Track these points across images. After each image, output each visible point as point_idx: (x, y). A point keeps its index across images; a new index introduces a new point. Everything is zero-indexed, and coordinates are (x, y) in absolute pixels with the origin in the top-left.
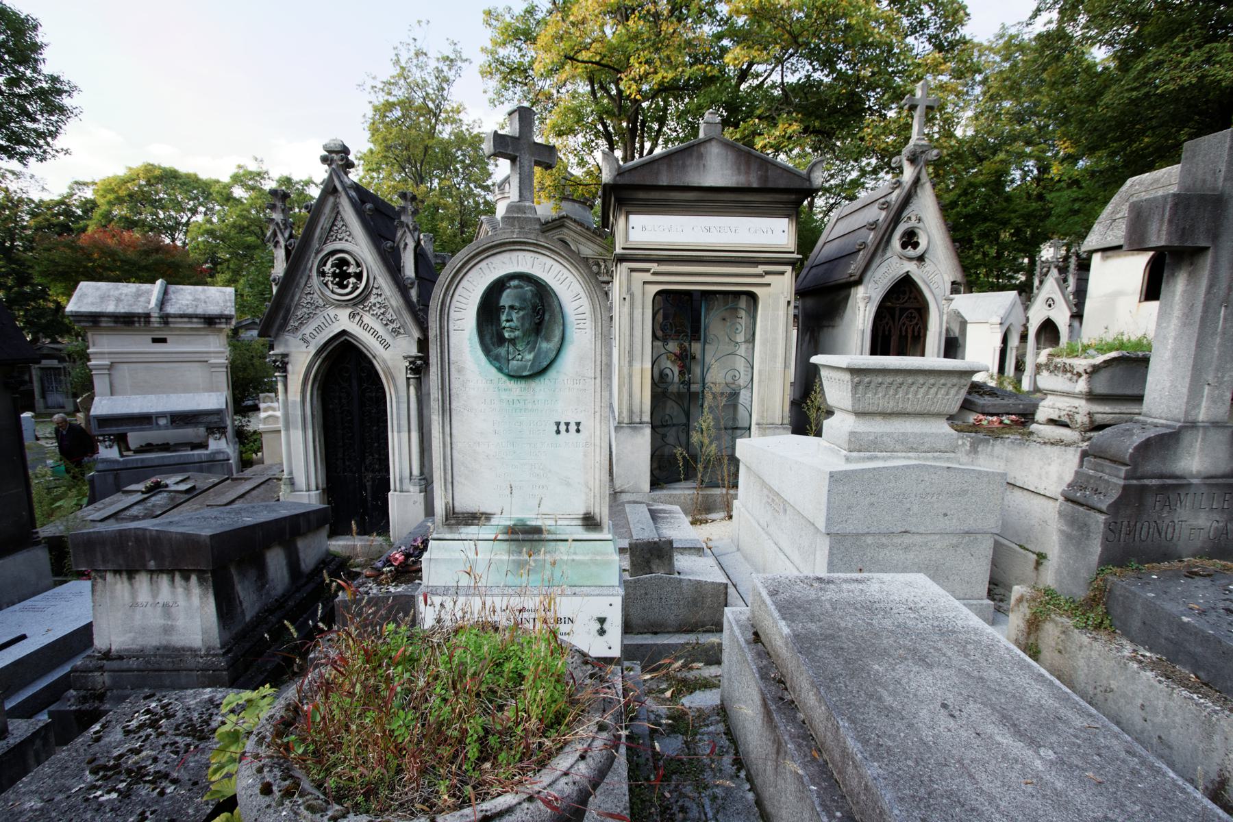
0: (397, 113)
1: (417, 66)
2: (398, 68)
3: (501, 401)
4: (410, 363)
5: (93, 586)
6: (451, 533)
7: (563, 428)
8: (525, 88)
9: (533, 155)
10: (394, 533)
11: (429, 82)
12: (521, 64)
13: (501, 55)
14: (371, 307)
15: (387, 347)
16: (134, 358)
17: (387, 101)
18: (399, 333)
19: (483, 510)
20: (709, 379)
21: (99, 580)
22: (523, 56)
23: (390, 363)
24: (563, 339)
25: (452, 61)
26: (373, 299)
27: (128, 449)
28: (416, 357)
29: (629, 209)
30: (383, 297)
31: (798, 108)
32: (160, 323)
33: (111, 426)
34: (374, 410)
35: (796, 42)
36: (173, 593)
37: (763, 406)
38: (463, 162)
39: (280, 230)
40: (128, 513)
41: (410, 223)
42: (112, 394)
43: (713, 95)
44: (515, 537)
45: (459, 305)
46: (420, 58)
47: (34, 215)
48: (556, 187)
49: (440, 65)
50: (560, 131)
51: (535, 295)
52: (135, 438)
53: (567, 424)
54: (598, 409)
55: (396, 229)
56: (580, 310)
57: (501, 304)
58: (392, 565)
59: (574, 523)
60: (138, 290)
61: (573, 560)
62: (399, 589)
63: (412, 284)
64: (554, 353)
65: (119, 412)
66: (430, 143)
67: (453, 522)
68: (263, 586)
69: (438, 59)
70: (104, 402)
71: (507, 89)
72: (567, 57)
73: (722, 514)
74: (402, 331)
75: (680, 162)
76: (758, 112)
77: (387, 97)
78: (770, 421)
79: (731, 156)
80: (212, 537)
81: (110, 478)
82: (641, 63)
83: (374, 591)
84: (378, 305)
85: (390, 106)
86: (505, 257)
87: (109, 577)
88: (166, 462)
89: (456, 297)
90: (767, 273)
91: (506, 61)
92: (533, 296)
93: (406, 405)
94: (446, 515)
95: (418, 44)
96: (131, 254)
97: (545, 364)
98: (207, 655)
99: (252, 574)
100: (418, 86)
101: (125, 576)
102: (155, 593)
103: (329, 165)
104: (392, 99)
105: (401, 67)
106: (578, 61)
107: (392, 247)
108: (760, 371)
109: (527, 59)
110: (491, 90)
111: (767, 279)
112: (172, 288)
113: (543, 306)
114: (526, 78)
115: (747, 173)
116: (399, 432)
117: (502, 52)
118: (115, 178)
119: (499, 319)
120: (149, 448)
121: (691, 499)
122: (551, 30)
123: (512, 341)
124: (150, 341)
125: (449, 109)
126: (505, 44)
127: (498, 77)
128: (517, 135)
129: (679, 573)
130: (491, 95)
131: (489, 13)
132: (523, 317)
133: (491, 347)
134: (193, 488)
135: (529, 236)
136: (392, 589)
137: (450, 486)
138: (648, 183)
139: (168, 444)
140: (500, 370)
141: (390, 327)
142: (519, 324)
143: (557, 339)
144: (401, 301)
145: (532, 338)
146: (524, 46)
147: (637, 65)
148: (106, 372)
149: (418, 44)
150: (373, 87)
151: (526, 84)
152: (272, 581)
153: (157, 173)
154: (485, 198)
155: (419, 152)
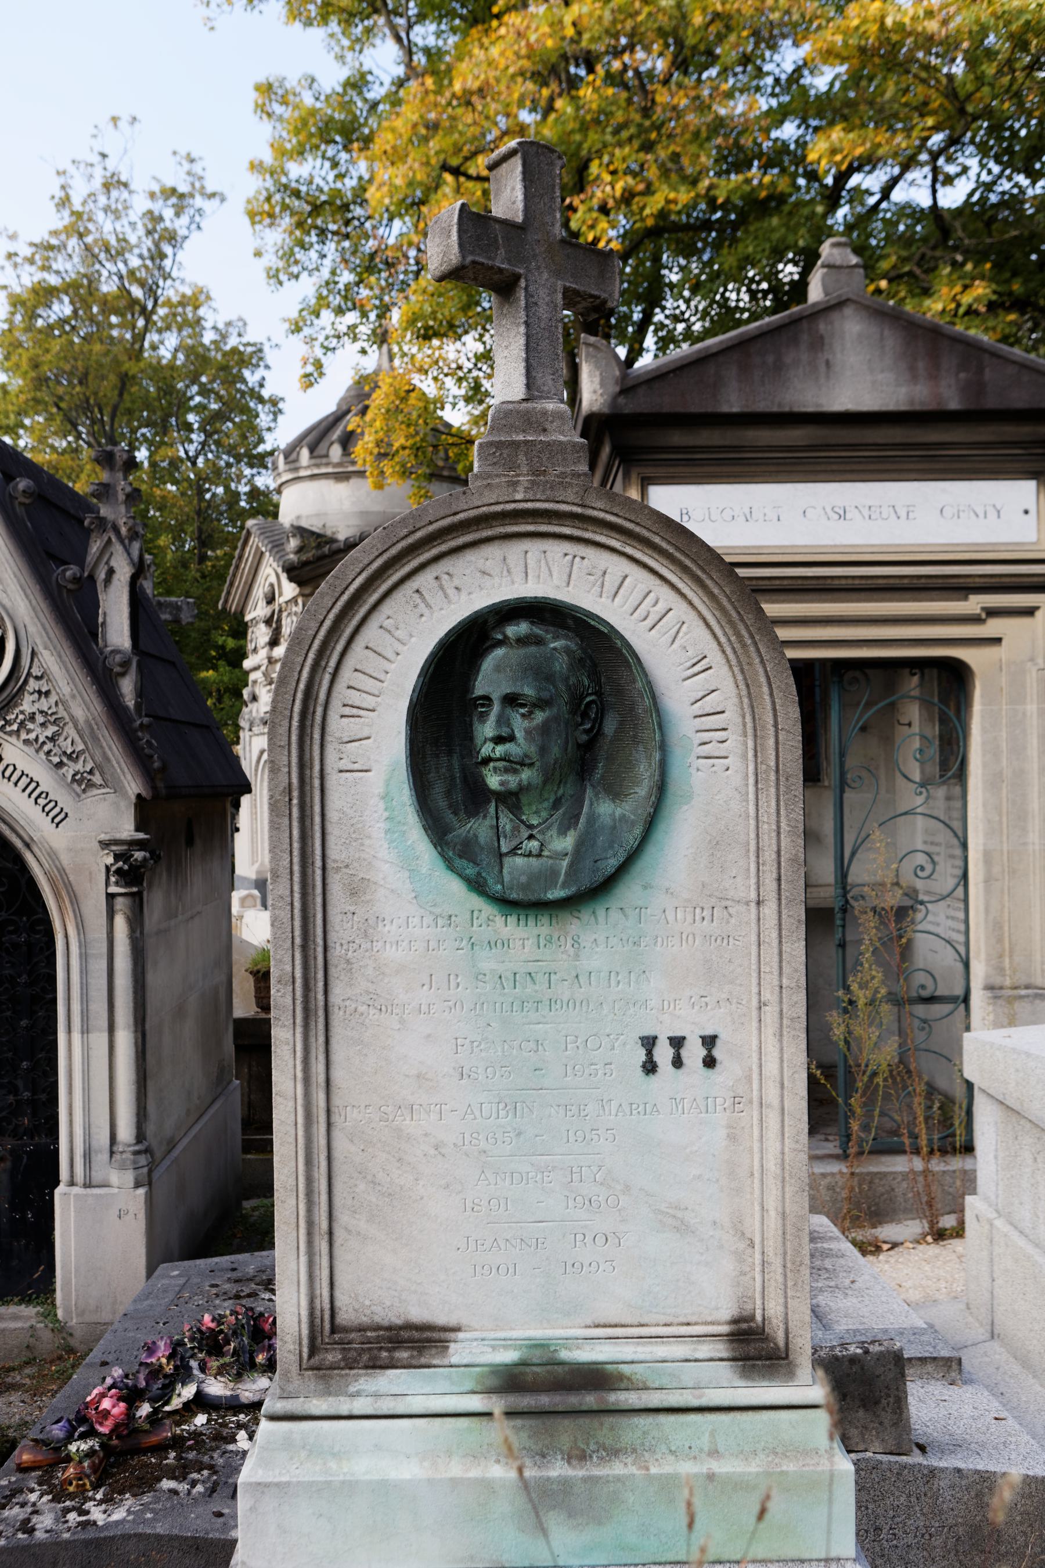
0: (62, 308)
1: (106, 209)
2: (66, 213)
4: (117, 857)
6: (328, 1393)
7: (663, 1054)
8: (346, 244)
9: (558, 274)
10: (67, 1297)
11: (133, 239)
12: (337, 193)
14: (22, 724)
15: (59, 819)
18: (91, 785)
19: (417, 1314)
20: (858, 874)
22: (340, 176)
23: (65, 860)
24: (661, 788)
25: (182, 196)
26: (27, 705)
28: (133, 844)
29: (649, 471)
30: (53, 698)
31: (979, 256)
34: (23, 979)
35: (962, 111)
37: (1000, 940)
38: (200, 408)
41: (121, 522)
43: (776, 236)
44: (526, 1401)
45: (355, 697)
46: (114, 193)
48: (417, 449)
49: (157, 207)
50: (427, 328)
51: (578, 663)
53: (677, 1043)
54: (769, 995)
55: (86, 535)
56: (710, 703)
58: (91, 1433)
59: (705, 1350)
61: (711, 1477)
62: (118, 1515)
63: (125, 664)
64: (638, 831)
66: (130, 367)
67: (332, 1357)
69: (152, 195)
71: (304, 246)
72: (445, 167)
73: (913, 1227)
74: (97, 779)
75: (770, 359)
76: (885, 265)
77: (39, 276)
78: (1023, 980)
79: (892, 340)
82: (613, 173)
83: (45, 1522)
84: (40, 719)
85: (45, 294)
86: (490, 556)
89: (347, 675)
90: (993, 613)
91: (304, 189)
93: (104, 964)
94: (312, 1338)
95: (111, 164)
97: (612, 863)
100: (107, 250)
104: (53, 280)
105: (73, 213)
106: (469, 177)
107: (76, 580)
108: (988, 857)
109: (350, 183)
110: (272, 250)
111: (993, 627)
113: (599, 693)
114: (347, 223)
115: (934, 376)
116: (85, 1031)
117: (297, 171)
119: (469, 736)
121: (831, 1188)
122: (409, 113)
123: (510, 799)
125: (175, 299)
126: (301, 153)
127: (287, 221)
128: (519, 218)
129: (922, 1448)
130: (270, 259)
131: (266, 89)
132: (545, 729)
133: (450, 817)
135: (560, 495)
136: (97, 1514)
138: (694, 409)
140: (477, 886)
141: (69, 771)
142: (533, 750)
143: (642, 790)
144: (97, 707)
145: (568, 789)
146: (344, 156)
147: (607, 178)
149: (111, 164)
151: (347, 236)
154: (250, 482)
155: (107, 387)
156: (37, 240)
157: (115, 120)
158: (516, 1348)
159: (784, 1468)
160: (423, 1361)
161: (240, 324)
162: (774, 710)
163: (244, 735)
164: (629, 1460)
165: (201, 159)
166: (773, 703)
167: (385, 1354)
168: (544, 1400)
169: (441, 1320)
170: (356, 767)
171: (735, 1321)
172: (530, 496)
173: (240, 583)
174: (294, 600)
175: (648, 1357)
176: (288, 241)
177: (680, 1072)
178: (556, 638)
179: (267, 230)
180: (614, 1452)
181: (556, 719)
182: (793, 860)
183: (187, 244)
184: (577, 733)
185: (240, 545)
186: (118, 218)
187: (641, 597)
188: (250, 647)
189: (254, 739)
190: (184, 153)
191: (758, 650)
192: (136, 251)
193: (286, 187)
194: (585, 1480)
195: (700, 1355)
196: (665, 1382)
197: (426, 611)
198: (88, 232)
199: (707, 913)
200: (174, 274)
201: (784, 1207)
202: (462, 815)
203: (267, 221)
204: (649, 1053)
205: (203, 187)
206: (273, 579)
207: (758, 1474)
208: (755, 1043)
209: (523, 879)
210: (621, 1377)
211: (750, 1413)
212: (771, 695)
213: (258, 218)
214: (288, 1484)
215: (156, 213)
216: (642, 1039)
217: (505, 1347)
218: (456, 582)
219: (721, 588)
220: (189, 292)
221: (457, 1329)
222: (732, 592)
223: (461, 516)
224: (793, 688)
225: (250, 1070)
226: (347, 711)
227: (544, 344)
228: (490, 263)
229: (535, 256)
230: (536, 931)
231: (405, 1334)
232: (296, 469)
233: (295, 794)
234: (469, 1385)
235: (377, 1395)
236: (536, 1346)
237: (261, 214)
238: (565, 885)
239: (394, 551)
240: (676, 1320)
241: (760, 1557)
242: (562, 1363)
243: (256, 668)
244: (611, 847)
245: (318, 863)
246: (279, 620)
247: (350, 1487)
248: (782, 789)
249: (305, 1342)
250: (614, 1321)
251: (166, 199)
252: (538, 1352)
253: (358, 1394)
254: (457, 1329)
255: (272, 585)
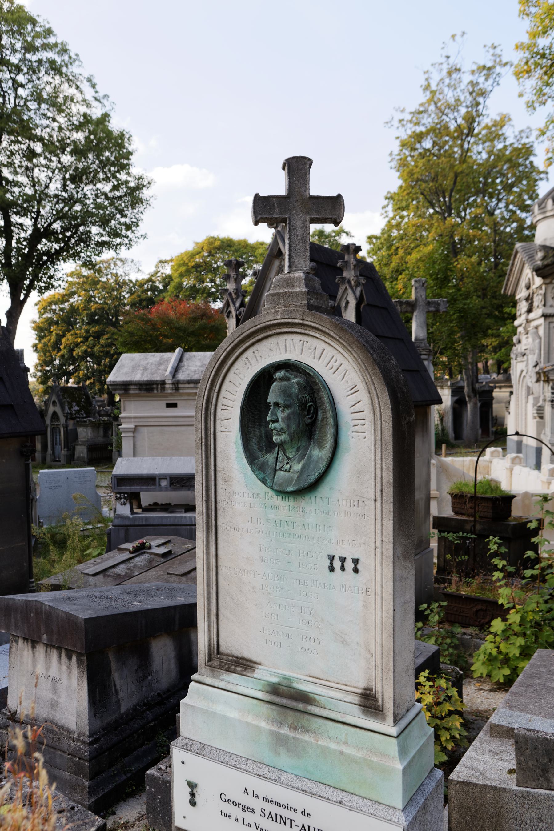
1: (449, 86)
2: (428, 93)
3: (268, 520)
5: (11, 648)
6: (213, 677)
7: (337, 564)
9: (308, 213)
11: (462, 99)
13: (541, 47)
16: (152, 422)
17: (414, 132)
21: (14, 644)
25: (489, 69)
27: (140, 506)
32: (172, 389)
33: (126, 485)
36: (60, 669)
39: (232, 300)
40: (114, 571)
42: (134, 455)
44: (277, 700)
45: (225, 402)
47: (131, 293)
49: (474, 78)
52: (146, 498)
53: (343, 560)
55: (337, 287)
56: (357, 408)
57: (268, 401)
60: (161, 358)
61: (341, 753)
65: (126, 472)
67: (216, 663)
68: (145, 677)
70: (124, 462)
80: (88, 621)
81: (122, 534)
85: (419, 137)
86: (263, 347)
87: (20, 641)
88: (165, 522)
89: (223, 393)
91: (547, 52)
92: (300, 390)
96: (183, 322)
98: (78, 740)
99: (133, 663)
101: (30, 644)
102: (48, 667)
103: (275, 228)
112: (187, 355)
113: (315, 402)
118: (186, 253)
120: (154, 507)
123: (281, 445)
124: (165, 405)
127: (539, 72)
130: (529, 96)
132: (288, 418)
133: (258, 453)
134: (169, 553)
135: (294, 315)
137: (214, 619)
139: (170, 504)
142: (284, 426)
143: (328, 445)
145: (303, 443)
148: (131, 434)
150: (401, 121)
152: (157, 672)
153: (217, 244)
156: (413, 110)
157: (453, 36)
158: (278, 677)
159: (372, 759)
160: (245, 673)
161: (528, 130)
162: (380, 411)
163: (513, 362)
164: (312, 736)
165: (499, 45)
166: (380, 408)
167: (233, 667)
168: (284, 701)
169: (254, 659)
170: (226, 430)
171: (366, 689)
172: (283, 317)
173: (513, 279)
174: (540, 287)
175: (326, 695)
176: (539, 83)
177: (344, 573)
178: (296, 377)
179: (527, 80)
180: (307, 731)
181: (293, 413)
182: (388, 482)
183: (491, 95)
184: (305, 419)
185: (512, 258)
186: (455, 89)
187: (330, 359)
188: (518, 314)
189: (519, 364)
190: (489, 44)
191: (374, 384)
192: (464, 104)
193: (537, 53)
194: (294, 738)
195: (346, 700)
196: (332, 707)
197: (250, 366)
198: (439, 100)
199: (356, 503)
200: (484, 113)
201: (382, 642)
202: (264, 452)
203: (526, 76)
204: (331, 562)
205: (501, 61)
206: (530, 276)
207: (360, 758)
208: (373, 565)
209: (281, 481)
210: (315, 700)
211: (363, 731)
212: (379, 404)
213: (521, 75)
214: (195, 707)
215: (475, 82)
216: (329, 556)
217: (275, 676)
218: (260, 354)
219: (358, 355)
220: (498, 119)
221: (259, 664)
222: (363, 357)
223: (258, 327)
224: (389, 402)
225: (445, 543)
226: (224, 407)
227: (300, 246)
228: (270, 216)
229: (295, 208)
230: (288, 503)
231: (241, 661)
232: (545, 212)
233: (203, 440)
234: (260, 687)
235: (229, 682)
236: (286, 678)
237: (522, 72)
238: (294, 485)
239: (235, 343)
240: (341, 682)
241: (361, 795)
242: (293, 688)
243: (520, 325)
244: (314, 470)
245: (213, 468)
246: (532, 298)
247: (213, 715)
248: (383, 449)
249: (207, 655)
250: (317, 676)
251: (480, 73)
252: (285, 681)
253: (222, 680)
254: (259, 664)
255: (529, 279)
